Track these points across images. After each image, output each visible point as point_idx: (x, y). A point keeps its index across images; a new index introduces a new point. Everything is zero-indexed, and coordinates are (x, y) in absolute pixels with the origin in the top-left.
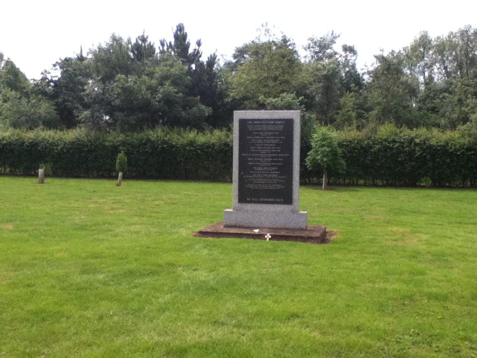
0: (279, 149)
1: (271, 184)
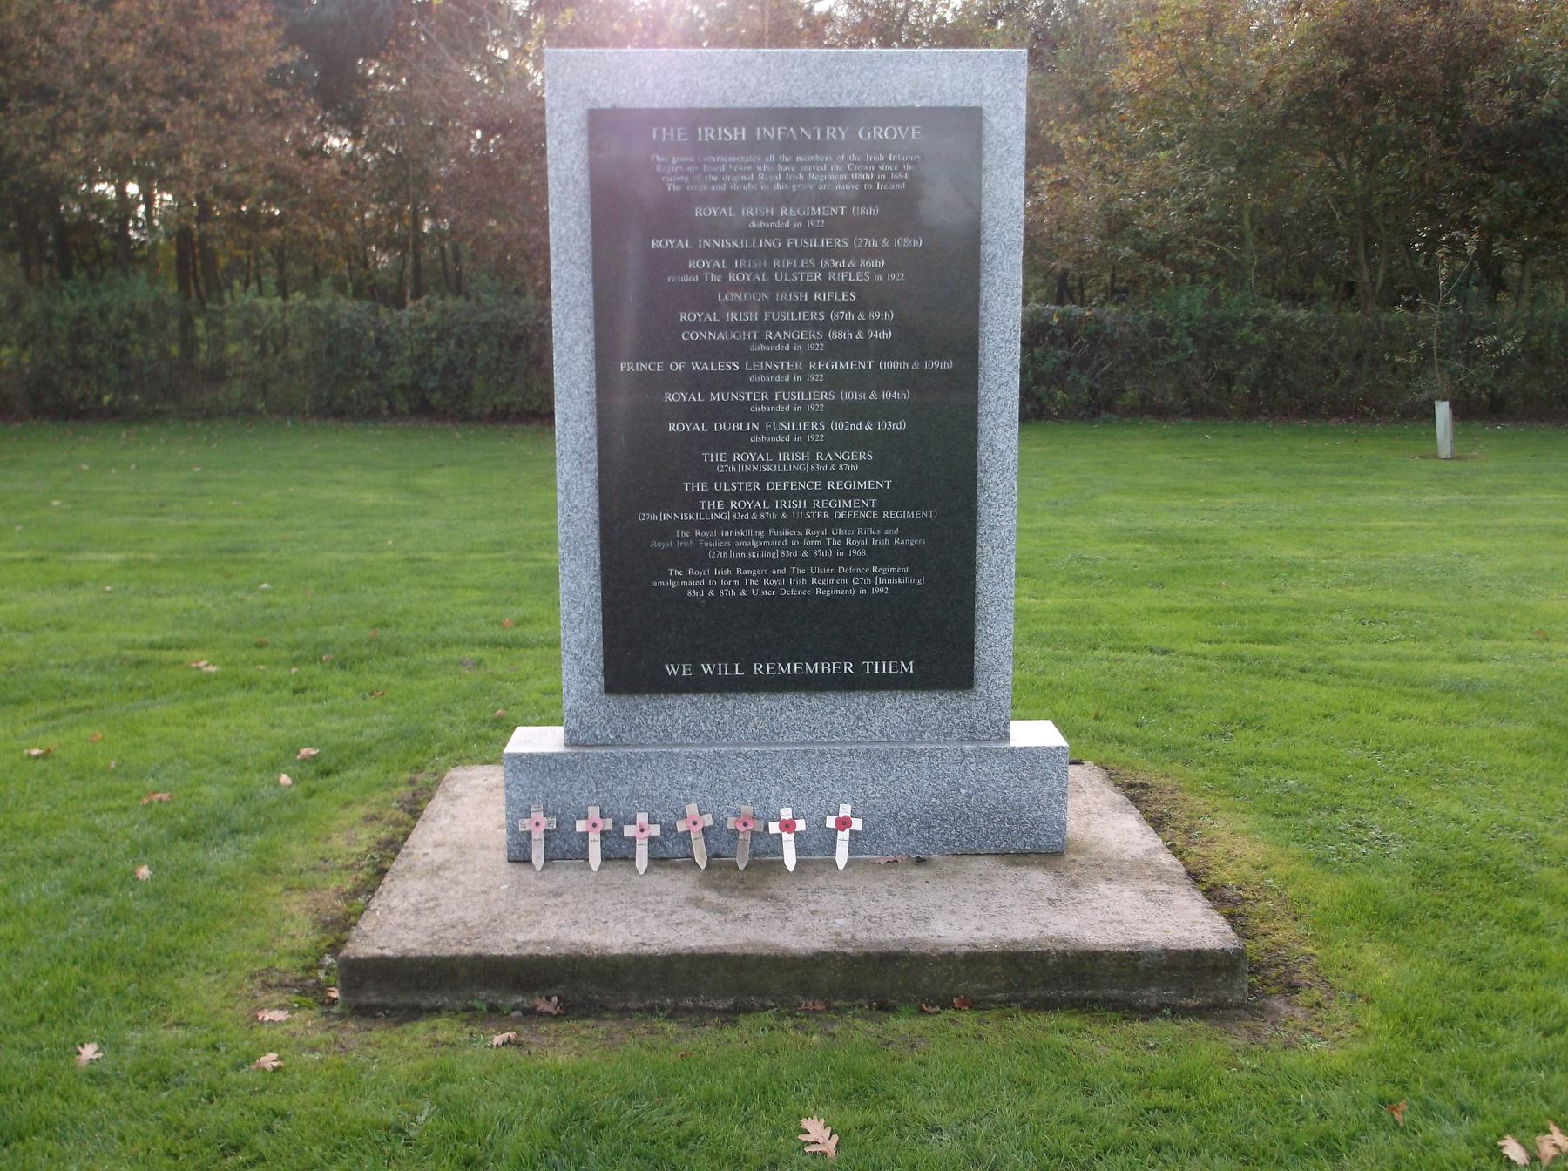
0: (880, 325)
1: (833, 562)
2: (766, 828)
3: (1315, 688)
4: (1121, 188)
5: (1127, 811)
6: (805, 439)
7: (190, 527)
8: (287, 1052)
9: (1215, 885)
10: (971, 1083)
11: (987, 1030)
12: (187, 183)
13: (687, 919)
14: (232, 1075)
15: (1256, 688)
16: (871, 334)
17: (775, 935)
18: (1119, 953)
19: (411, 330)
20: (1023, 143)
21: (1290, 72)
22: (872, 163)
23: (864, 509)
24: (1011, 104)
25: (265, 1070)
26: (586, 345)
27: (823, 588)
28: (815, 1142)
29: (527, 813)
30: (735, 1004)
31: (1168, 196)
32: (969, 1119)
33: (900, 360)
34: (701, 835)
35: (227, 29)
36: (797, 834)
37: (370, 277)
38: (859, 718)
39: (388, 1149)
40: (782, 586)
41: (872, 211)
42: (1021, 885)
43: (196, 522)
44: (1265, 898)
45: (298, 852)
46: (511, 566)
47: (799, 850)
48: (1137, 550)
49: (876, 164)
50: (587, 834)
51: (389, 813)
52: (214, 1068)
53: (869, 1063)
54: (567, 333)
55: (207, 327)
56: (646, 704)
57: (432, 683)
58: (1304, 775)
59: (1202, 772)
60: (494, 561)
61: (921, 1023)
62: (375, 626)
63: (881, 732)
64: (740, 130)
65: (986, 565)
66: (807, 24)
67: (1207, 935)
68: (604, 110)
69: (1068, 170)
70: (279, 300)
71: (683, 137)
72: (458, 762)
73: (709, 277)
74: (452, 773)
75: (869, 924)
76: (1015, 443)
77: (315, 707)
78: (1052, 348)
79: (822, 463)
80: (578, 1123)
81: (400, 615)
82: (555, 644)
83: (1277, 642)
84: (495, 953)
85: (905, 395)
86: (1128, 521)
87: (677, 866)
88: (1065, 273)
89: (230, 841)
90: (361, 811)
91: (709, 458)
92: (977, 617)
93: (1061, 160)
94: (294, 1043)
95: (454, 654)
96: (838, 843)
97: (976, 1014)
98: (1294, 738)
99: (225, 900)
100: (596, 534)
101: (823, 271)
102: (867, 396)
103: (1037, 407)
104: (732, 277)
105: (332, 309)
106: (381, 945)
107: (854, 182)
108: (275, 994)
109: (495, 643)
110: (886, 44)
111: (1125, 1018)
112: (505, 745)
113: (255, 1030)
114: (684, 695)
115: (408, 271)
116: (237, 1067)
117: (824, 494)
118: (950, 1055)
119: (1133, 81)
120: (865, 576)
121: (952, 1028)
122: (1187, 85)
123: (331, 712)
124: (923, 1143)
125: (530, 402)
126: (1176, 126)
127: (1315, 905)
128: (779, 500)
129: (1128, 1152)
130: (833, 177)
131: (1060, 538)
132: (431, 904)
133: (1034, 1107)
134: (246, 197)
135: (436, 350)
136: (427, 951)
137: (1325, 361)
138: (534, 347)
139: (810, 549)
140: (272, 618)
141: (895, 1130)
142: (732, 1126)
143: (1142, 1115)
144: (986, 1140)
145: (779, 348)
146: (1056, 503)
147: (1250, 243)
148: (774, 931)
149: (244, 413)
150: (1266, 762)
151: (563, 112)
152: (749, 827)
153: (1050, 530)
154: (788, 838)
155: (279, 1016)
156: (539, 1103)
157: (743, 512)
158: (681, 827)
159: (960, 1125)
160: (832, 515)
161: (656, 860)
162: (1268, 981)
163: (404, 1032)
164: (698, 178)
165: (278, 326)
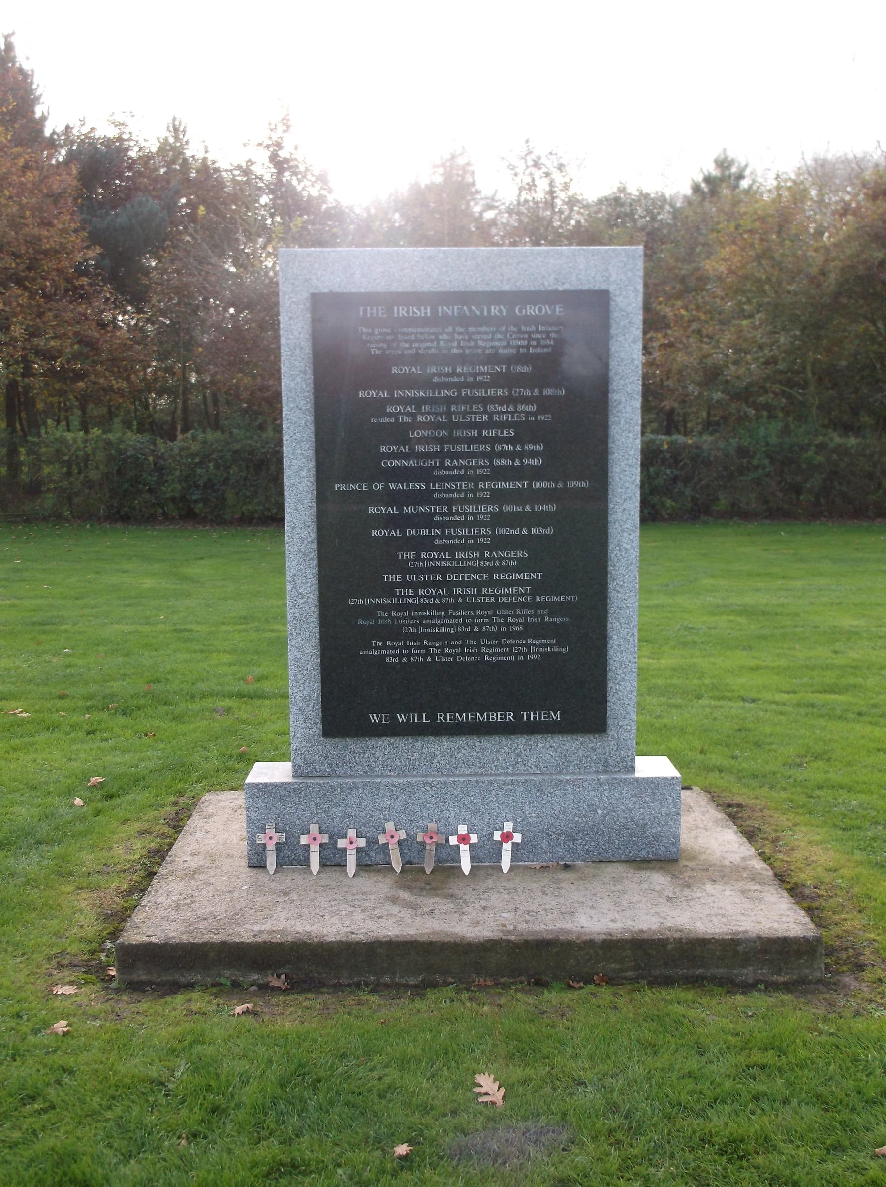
0: (533, 454)
1: (498, 636)
2: (447, 841)
3: (869, 728)
4: (714, 347)
5: (728, 827)
6: (476, 542)
7: (11, 606)
8: (75, 1020)
9: (796, 884)
10: (609, 1045)
11: (621, 1002)
12: (15, 347)
13: (386, 913)
14: (32, 1039)
15: (824, 728)
16: (526, 461)
17: (454, 926)
18: (723, 939)
19: (181, 456)
20: (641, 317)
21: (840, 261)
22: (526, 332)
23: (522, 595)
24: (631, 288)
25: (57, 1034)
26: (309, 470)
27: (490, 655)
28: (487, 1094)
29: (263, 830)
30: (423, 980)
31: (749, 353)
32: (607, 1074)
33: (549, 481)
34: (397, 846)
35: (46, 233)
36: (471, 846)
37: (150, 416)
38: (519, 755)
39: (151, 1099)
40: (458, 654)
41: (526, 369)
42: (645, 886)
43: (16, 602)
44: (836, 895)
45: (87, 859)
46: (253, 635)
47: (473, 858)
48: (731, 621)
49: (529, 333)
50: (308, 846)
51: (158, 828)
52: (17, 1032)
53: (529, 1030)
54: (295, 462)
55: (28, 455)
56: (354, 745)
57: (192, 726)
58: (863, 797)
59: (783, 795)
60: (240, 631)
61: (569, 996)
62: (150, 682)
63: (536, 766)
64: (426, 309)
65: (615, 637)
66: (478, 228)
67: (792, 925)
68: (324, 294)
69: (674, 333)
70: (81, 433)
71: (383, 314)
72: (211, 789)
73: (402, 418)
74: (207, 797)
75: (527, 917)
76: (636, 543)
77: (103, 745)
78: (663, 468)
79: (489, 560)
80: (300, 1078)
81: (169, 673)
82: (285, 696)
83: (839, 692)
84: (237, 941)
85: (552, 508)
86: (723, 599)
87: (379, 871)
88: (672, 410)
89: (34, 851)
90: (137, 826)
91: (402, 556)
92: (609, 677)
93: (668, 327)
94: (80, 1012)
95: (208, 703)
96: (503, 852)
97: (612, 989)
98: (855, 768)
99: (30, 898)
100: (316, 614)
101: (489, 414)
102: (523, 509)
103: (652, 512)
104: (420, 419)
105: (121, 441)
106: (150, 934)
107: (513, 347)
108: (67, 973)
109: (240, 695)
110: (537, 243)
111: (728, 992)
112: (247, 774)
113: (50, 1002)
114: (384, 738)
115: (179, 412)
116: (36, 1032)
117: (491, 583)
118: (592, 1022)
119: (722, 268)
120: (522, 645)
121: (594, 1001)
122: (762, 271)
123: (115, 748)
124: (571, 1094)
125: (269, 510)
126: (754, 301)
127: (875, 900)
128: (456, 588)
129: (733, 1101)
130: (497, 344)
131: (671, 612)
132: (188, 901)
133: (659, 1065)
134: (58, 358)
135: (199, 471)
136: (185, 938)
137: (870, 476)
138: (273, 468)
139: (480, 626)
140: (72, 676)
141: (550, 1084)
142: (420, 1080)
143: (744, 1071)
144: (621, 1092)
145: (456, 472)
146: (667, 586)
147: (812, 388)
148: (454, 923)
149: (55, 518)
150: (833, 787)
151: (292, 295)
152: (433, 840)
153: (663, 606)
154: (464, 849)
155: (69, 990)
156: (270, 1062)
157: (429, 597)
158: (382, 840)
159: (601, 1079)
160: (497, 599)
161: (363, 866)
162: (841, 962)
163: (166, 1003)
164: (395, 344)
165: (81, 453)
